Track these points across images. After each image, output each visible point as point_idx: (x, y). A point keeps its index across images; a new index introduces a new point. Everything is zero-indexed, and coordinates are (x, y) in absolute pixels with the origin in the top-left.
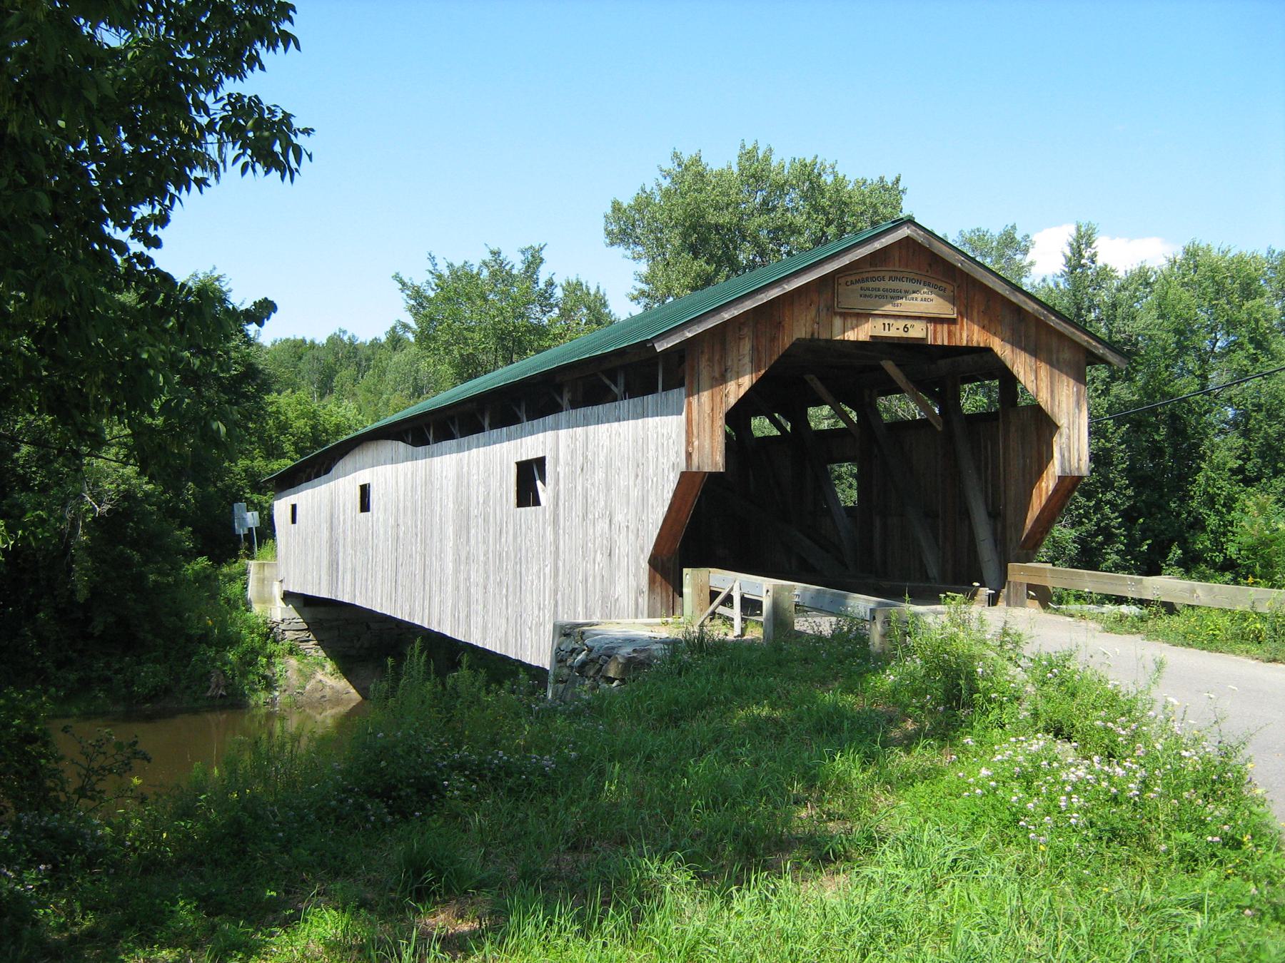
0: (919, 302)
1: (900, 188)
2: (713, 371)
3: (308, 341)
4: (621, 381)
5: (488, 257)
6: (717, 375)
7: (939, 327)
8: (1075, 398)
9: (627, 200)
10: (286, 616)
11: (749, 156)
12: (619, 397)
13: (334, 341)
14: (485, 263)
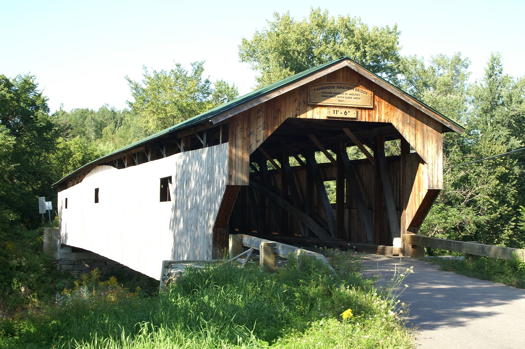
0: (353, 99)
1: (397, 31)
2: (244, 134)
3: (90, 110)
4: (205, 137)
5: (174, 68)
6: (245, 136)
7: (363, 112)
8: (436, 149)
9: (250, 39)
10: (63, 257)
11: (315, 14)
12: (204, 146)
13: (103, 111)
14: (172, 71)
